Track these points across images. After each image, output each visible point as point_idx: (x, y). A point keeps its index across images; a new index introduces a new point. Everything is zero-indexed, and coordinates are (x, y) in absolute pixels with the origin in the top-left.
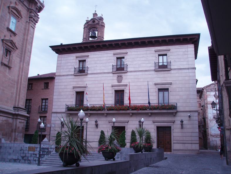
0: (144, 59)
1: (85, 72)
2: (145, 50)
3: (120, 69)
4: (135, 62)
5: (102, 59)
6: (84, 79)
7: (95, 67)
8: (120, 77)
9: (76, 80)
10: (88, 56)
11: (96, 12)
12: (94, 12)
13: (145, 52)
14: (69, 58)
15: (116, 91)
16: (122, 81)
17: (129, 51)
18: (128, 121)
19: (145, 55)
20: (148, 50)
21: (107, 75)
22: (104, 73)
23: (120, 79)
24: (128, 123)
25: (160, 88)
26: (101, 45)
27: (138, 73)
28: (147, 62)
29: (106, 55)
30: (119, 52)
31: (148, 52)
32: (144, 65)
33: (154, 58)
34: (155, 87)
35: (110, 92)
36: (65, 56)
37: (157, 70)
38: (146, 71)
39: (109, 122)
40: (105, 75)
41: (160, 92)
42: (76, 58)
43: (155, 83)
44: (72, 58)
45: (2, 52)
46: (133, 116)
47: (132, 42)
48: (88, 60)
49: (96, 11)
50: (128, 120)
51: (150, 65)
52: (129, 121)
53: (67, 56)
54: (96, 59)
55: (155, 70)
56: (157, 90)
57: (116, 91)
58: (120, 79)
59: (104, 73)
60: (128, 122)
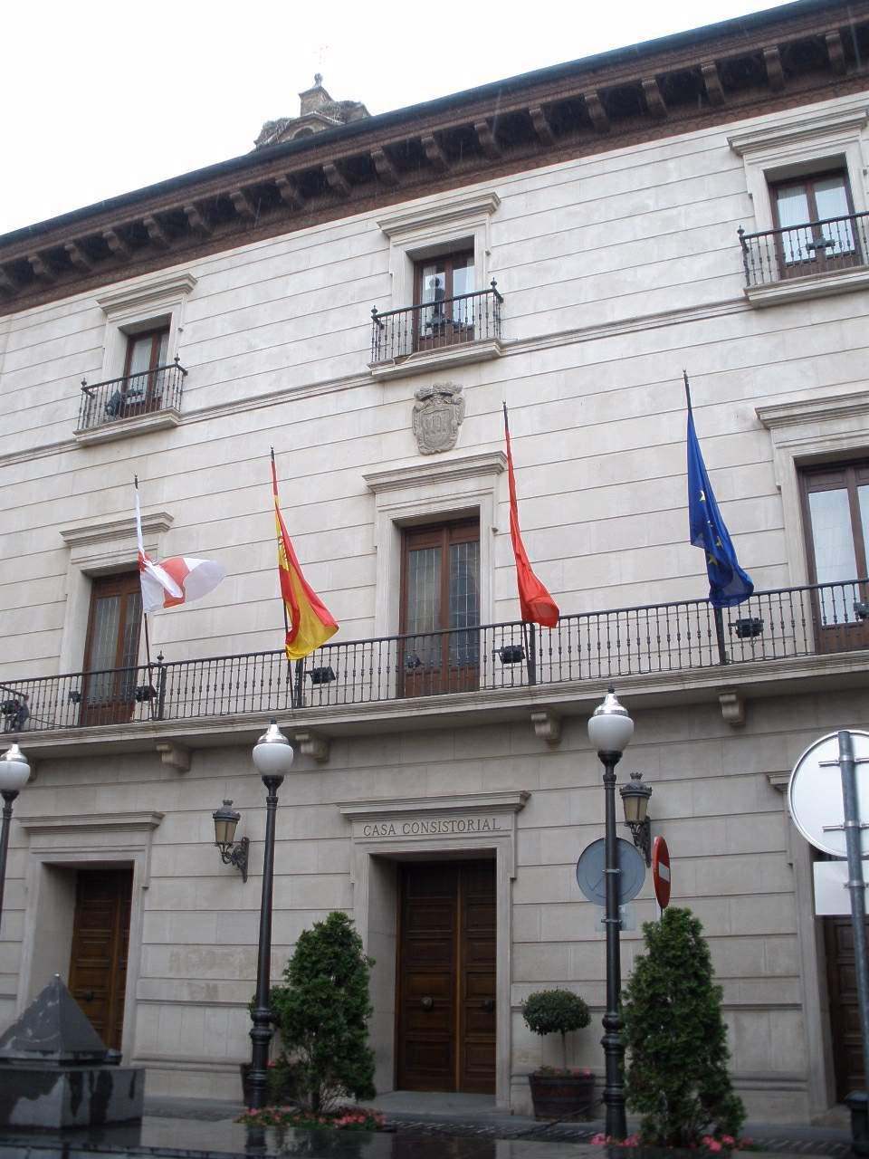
0: (640, 226)
1: (473, 684)
2: (656, 155)
3: (437, 337)
4: (568, 267)
5: (294, 284)
6: (153, 468)
7: (239, 361)
8: (438, 403)
9: (92, 479)
10: (186, 287)
11: (324, 85)
12: (310, 84)
13: (647, 176)
14: (57, 329)
15: (414, 533)
16: (455, 431)
17: (514, 188)
18: (526, 797)
19: (649, 200)
20: (668, 152)
21: (330, 403)
22: (309, 390)
23: (436, 420)
24: (524, 820)
25: (812, 450)
26: (281, 180)
27: (594, 350)
28: (671, 248)
29: (322, 255)
30: (430, 213)
31: (673, 170)
32: (647, 276)
33: (731, 210)
34: (762, 446)
35: (357, 543)
36: (34, 320)
37: (770, 294)
38: (669, 318)
39: (350, 819)
40: (313, 406)
41: (816, 499)
42: (106, 311)
43: (759, 411)
44: (75, 323)
45: (867, 1042)
46: (563, 747)
47: (526, 111)
48: (186, 316)
49: (318, 78)
50: (521, 787)
51: (699, 267)
52: (536, 799)
53: (52, 314)
54: (248, 297)
55: (746, 299)
56: (788, 476)
57: (414, 533)
58: (436, 420)
59: (309, 390)
60: (518, 809)
